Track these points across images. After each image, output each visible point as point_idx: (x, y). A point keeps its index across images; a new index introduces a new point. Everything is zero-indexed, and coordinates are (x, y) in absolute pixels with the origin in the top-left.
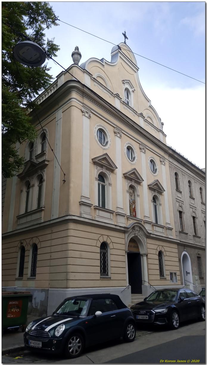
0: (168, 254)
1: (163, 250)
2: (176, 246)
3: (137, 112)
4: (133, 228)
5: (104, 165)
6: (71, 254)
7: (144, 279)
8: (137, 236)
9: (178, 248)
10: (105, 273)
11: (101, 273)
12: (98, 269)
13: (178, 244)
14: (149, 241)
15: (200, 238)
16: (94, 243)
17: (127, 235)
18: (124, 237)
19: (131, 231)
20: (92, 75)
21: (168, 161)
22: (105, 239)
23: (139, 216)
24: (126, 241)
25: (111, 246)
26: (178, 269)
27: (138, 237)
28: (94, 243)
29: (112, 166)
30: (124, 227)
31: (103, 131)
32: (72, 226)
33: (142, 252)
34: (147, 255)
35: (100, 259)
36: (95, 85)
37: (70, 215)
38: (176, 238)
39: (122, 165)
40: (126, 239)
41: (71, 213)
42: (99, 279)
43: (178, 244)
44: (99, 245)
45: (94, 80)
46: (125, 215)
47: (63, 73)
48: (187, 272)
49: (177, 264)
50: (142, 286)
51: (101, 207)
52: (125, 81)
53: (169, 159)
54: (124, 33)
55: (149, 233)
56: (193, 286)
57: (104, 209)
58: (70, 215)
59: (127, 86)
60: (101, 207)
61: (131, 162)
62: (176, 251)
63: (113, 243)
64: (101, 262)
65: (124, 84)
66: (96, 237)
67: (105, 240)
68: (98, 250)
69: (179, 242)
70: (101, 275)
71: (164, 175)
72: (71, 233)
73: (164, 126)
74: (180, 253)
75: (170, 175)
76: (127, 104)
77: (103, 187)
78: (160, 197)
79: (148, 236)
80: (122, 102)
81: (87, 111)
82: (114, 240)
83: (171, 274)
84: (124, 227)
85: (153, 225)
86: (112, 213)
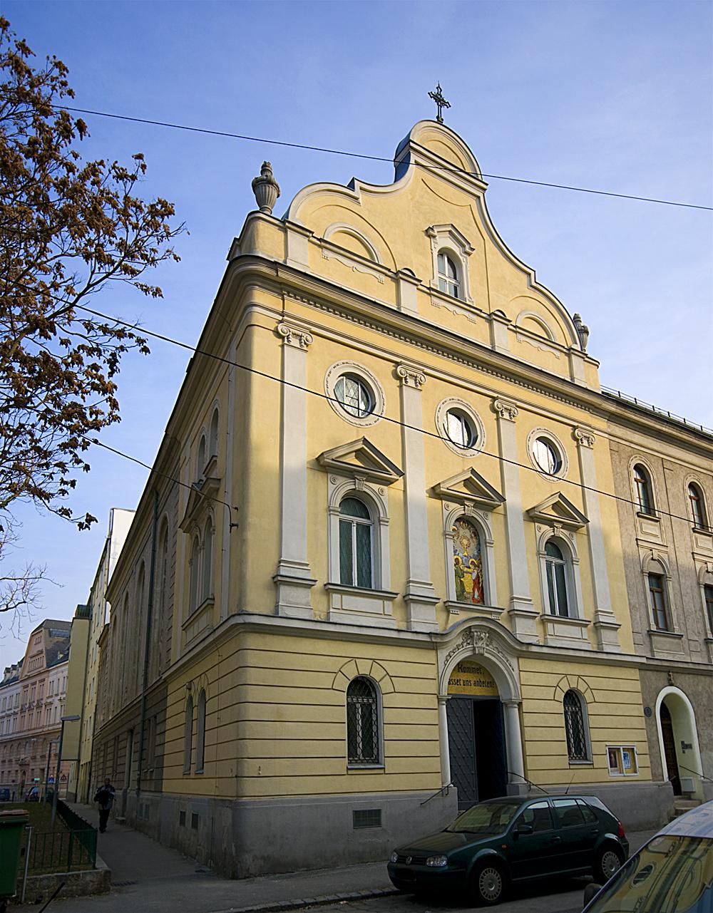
0: (599, 696)
1: (582, 687)
2: (635, 674)
3: (481, 311)
4: (468, 633)
5: (475, 504)
6: (252, 712)
7: (511, 769)
8: (483, 655)
9: (642, 680)
10: (580, 754)
11: (569, 754)
12: (563, 748)
13: (641, 667)
14: (526, 664)
15: (680, 639)
16: (549, 693)
17: (443, 654)
18: (435, 659)
19: (460, 641)
20: (313, 233)
21: (607, 436)
22: (364, 669)
23: (497, 598)
24: (440, 671)
25: (385, 686)
26: (643, 735)
27: (486, 655)
28: (549, 693)
29: (576, 519)
30: (430, 633)
31: (359, 380)
32: (253, 641)
33: (503, 697)
34: (521, 703)
35: (564, 725)
36: (519, 341)
37: (244, 614)
38: (636, 651)
39: (521, 494)
40: (441, 665)
41: (250, 610)
42: (346, 773)
43: (641, 667)
44: (561, 696)
45: (323, 244)
46: (536, 615)
47: (237, 242)
48: (683, 743)
49: (641, 722)
50: (507, 786)
51: (355, 588)
52: (436, 230)
53: (609, 431)
54: (435, 91)
55: (523, 643)
56: (703, 782)
57: (351, 587)
58: (244, 614)
59: (445, 242)
60: (355, 588)
61: (462, 451)
62: (637, 686)
63: (392, 678)
64: (568, 732)
65: (434, 237)
66: (553, 680)
67: (573, 686)
68: (343, 699)
69: (644, 660)
70: (571, 758)
71: (597, 476)
72: (252, 658)
73: (589, 339)
74: (649, 693)
75: (615, 473)
76: (457, 296)
77: (560, 568)
78: (576, 543)
79: (523, 651)
80: (318, 242)
81: (585, 435)
82: (393, 669)
83: (613, 752)
84: (429, 634)
85: (544, 622)
86: (392, 599)
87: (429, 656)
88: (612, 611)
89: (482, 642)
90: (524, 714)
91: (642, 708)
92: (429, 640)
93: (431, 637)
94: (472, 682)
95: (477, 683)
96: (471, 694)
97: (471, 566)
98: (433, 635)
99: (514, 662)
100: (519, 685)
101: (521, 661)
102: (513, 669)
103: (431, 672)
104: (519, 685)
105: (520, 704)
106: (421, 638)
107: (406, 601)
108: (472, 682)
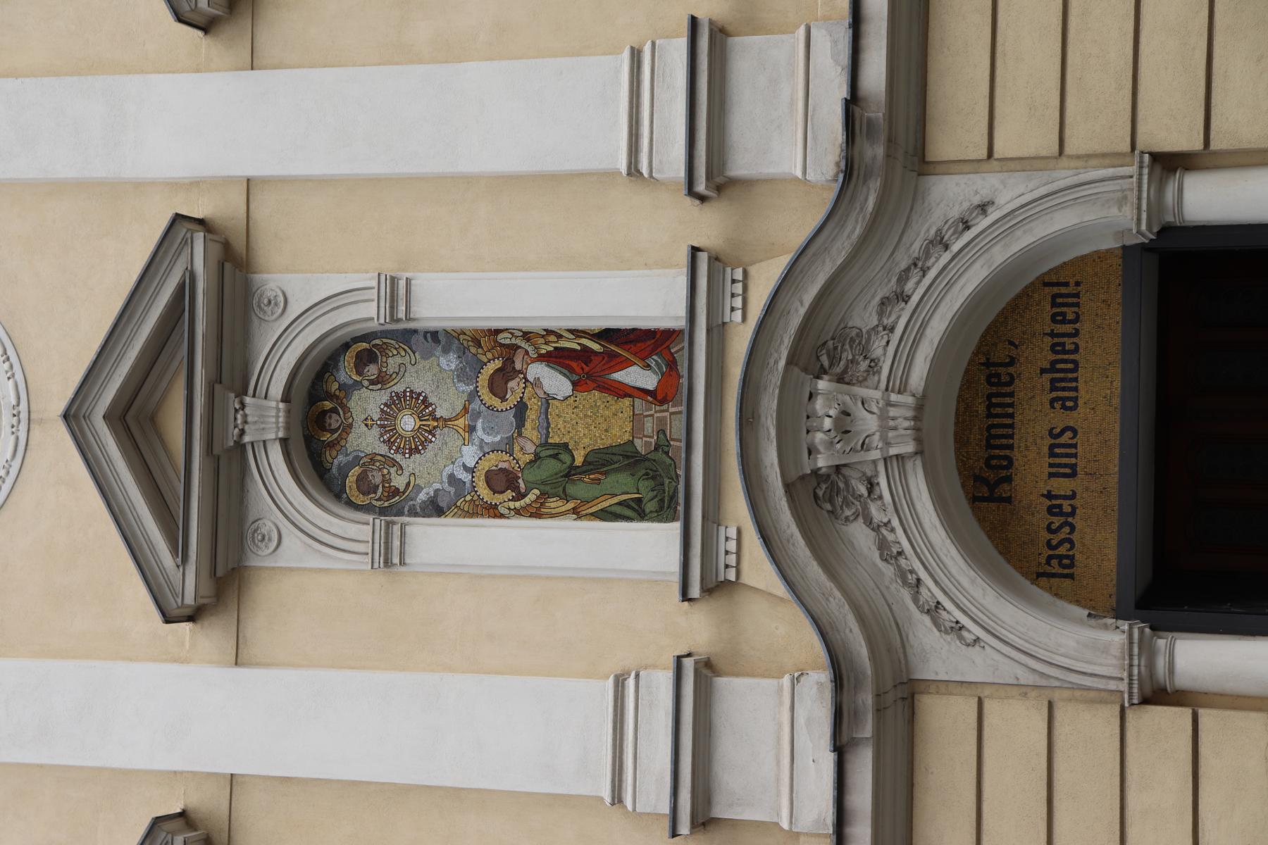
17: (937, 656)
29: (181, 288)
84: (841, 750)
87: (945, 721)
88: (626, 55)
89: (859, 412)
90: (1214, 146)
91: (1185, 139)
92: (875, 185)
93: (855, 743)
94: (1059, 419)
95: (1063, 380)
96: (1115, 437)
97: (512, 399)
98: (845, 739)
99: (949, 194)
100: (1064, 176)
101: (943, 146)
102: (983, 208)
103: (1016, 728)
104: (1064, 176)
105: (1169, 164)
106: (862, 798)
107: (719, 189)
108: (1059, 419)
